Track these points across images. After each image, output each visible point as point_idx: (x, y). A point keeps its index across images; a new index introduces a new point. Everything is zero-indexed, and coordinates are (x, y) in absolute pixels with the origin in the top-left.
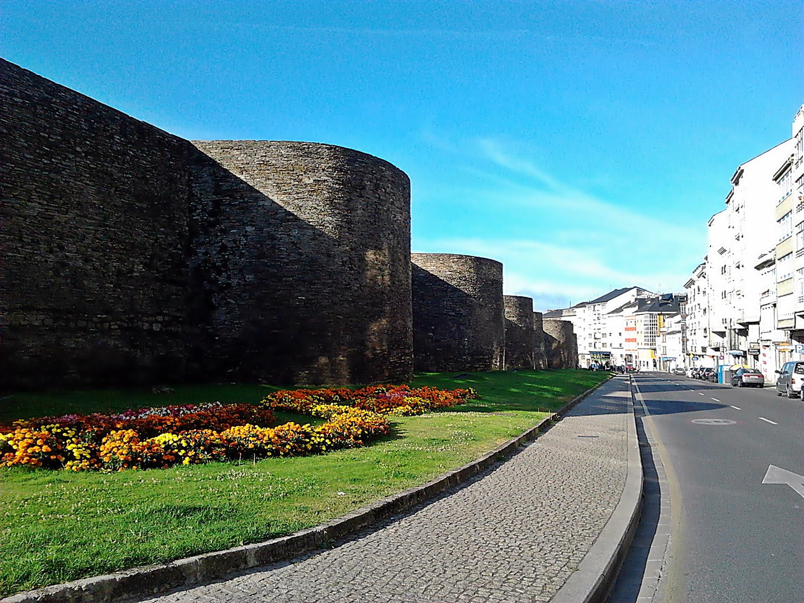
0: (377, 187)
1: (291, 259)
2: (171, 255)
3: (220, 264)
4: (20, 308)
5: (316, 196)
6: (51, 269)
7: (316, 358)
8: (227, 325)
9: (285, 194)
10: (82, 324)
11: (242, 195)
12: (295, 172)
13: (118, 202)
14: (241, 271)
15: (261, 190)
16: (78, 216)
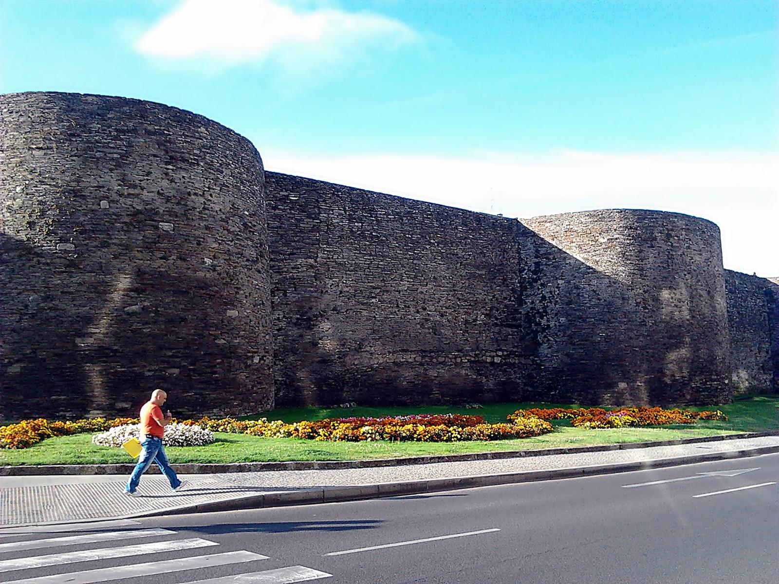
0: (669, 236)
1: (593, 303)
2: (506, 306)
3: (542, 310)
4: (400, 350)
5: (610, 251)
6: (418, 324)
7: (616, 383)
8: (549, 357)
9: (585, 252)
10: (441, 359)
11: (554, 256)
12: (592, 235)
13: (463, 273)
14: (556, 314)
15: (568, 251)
16: (435, 286)
